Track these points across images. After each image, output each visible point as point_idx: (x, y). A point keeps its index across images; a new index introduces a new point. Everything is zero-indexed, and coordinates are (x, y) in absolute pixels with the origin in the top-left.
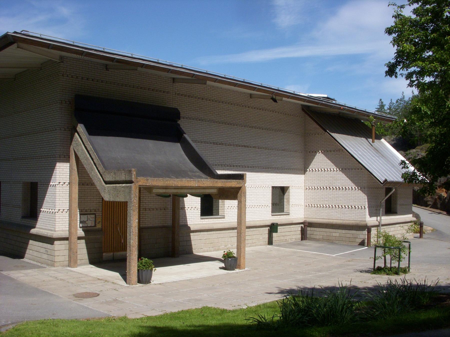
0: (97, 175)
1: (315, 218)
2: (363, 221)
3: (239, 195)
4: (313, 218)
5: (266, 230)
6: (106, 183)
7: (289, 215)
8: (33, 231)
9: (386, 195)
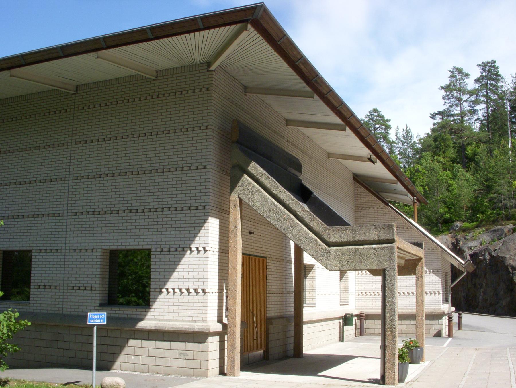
0: (307, 234)
1: (371, 309)
2: (437, 309)
3: (418, 268)
4: (368, 309)
5: (337, 323)
6: (329, 244)
7: (348, 305)
8: (142, 325)
9: (452, 281)
